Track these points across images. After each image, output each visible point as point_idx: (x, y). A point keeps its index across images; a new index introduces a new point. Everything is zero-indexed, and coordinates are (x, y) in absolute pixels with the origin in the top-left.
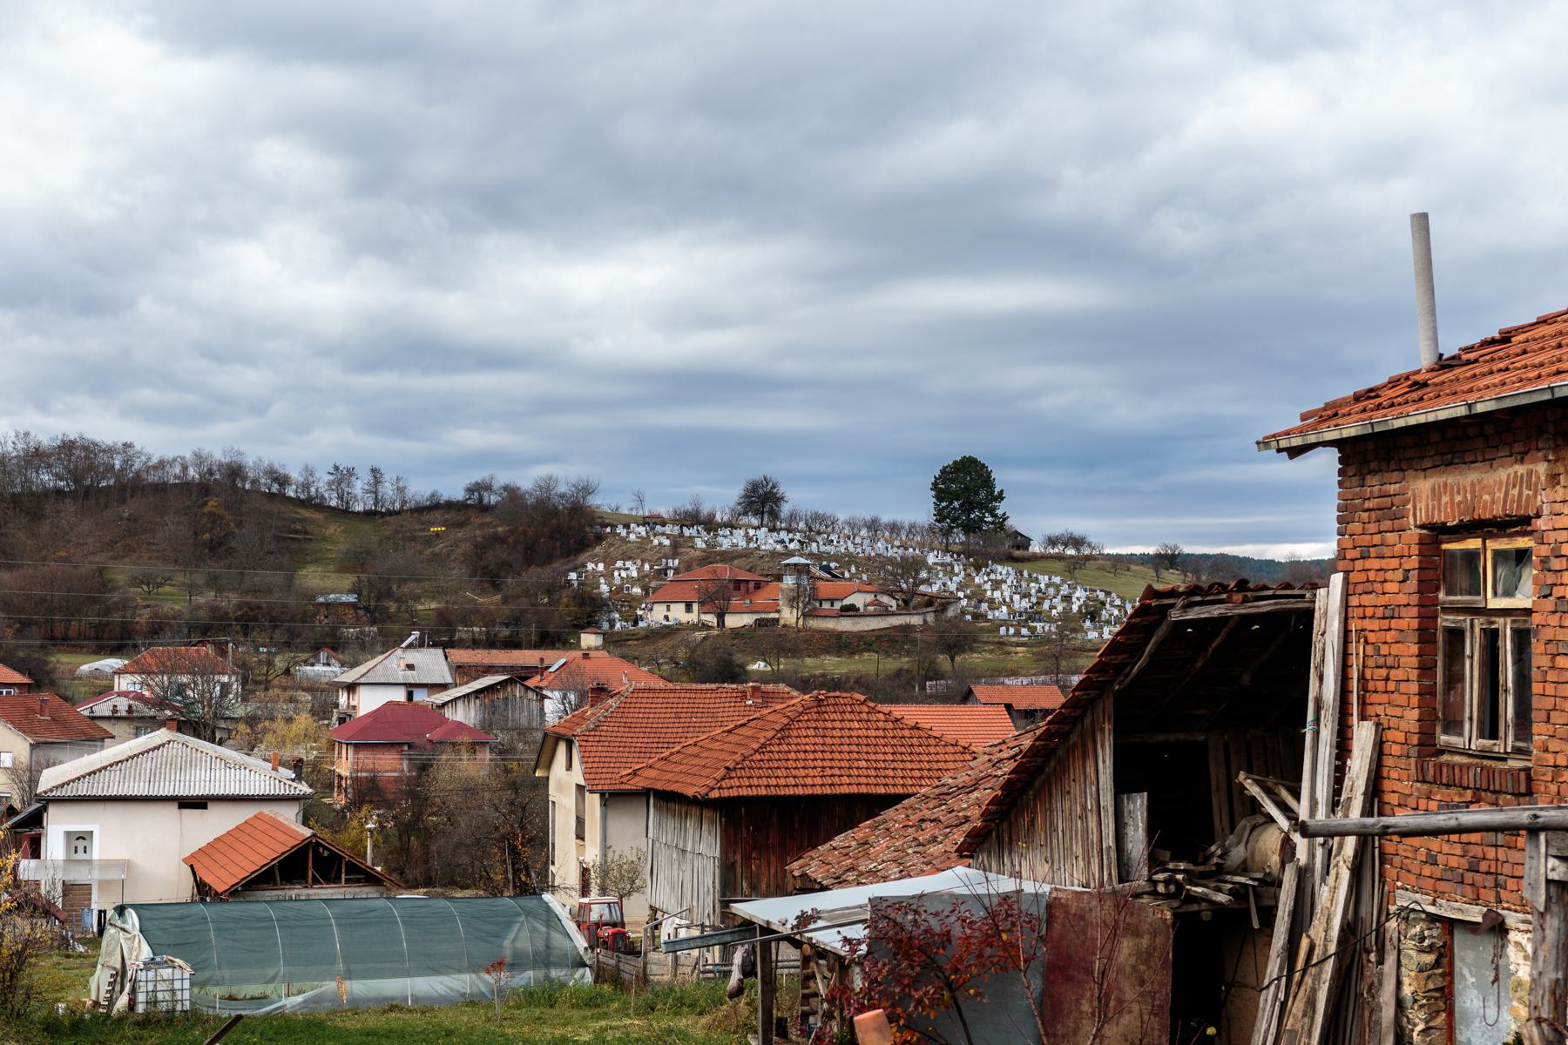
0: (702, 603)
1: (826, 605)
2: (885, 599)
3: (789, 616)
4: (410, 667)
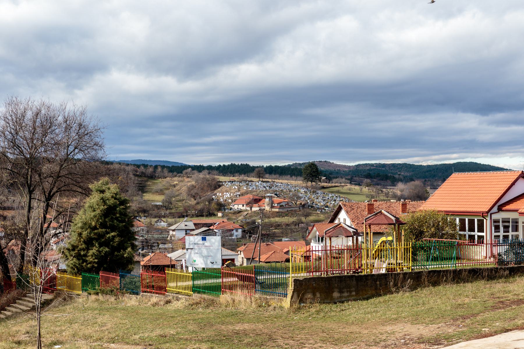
0: (246, 205)
3: (267, 208)
4: (186, 225)
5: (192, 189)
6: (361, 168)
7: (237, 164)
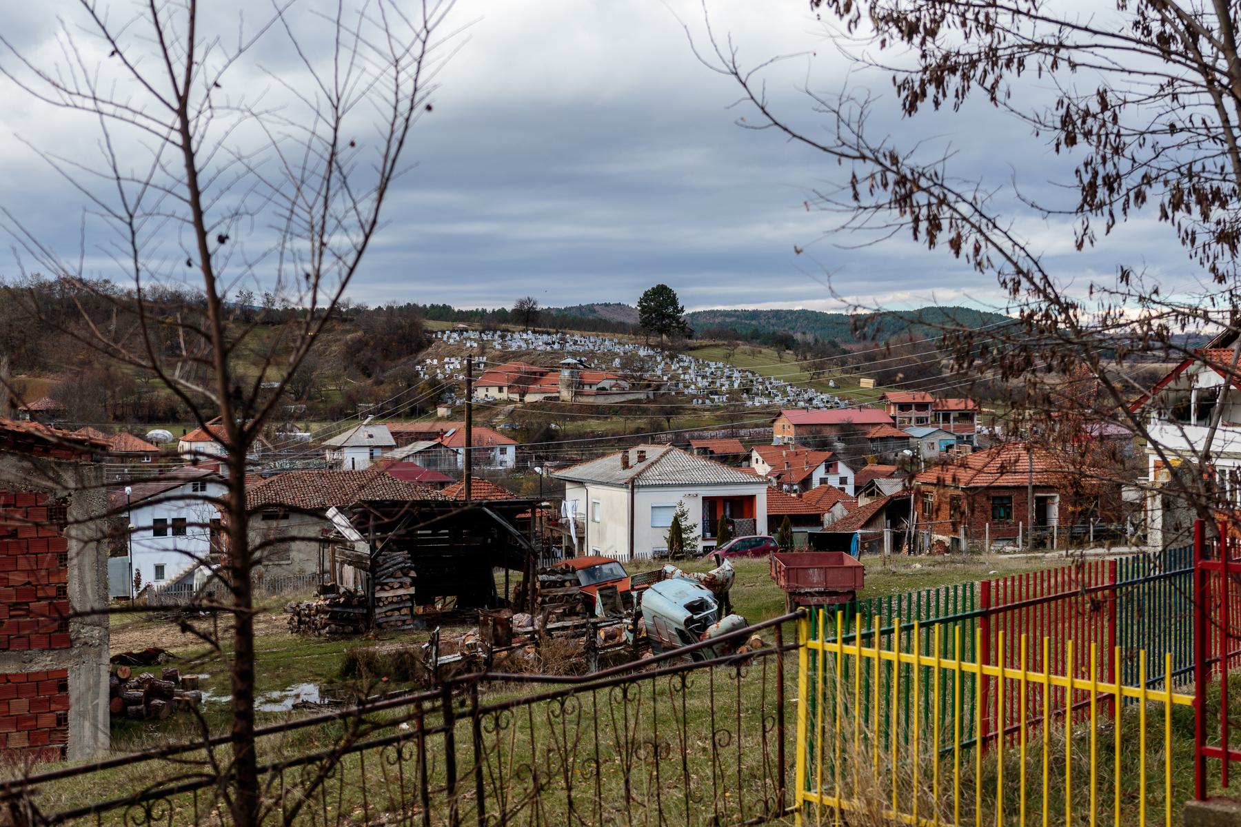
0: (509, 387)
1: (587, 388)
2: (623, 383)
3: (566, 395)
4: (371, 436)
5: (359, 351)
6: (702, 321)
7: (421, 305)
